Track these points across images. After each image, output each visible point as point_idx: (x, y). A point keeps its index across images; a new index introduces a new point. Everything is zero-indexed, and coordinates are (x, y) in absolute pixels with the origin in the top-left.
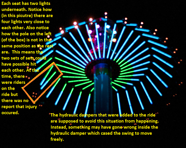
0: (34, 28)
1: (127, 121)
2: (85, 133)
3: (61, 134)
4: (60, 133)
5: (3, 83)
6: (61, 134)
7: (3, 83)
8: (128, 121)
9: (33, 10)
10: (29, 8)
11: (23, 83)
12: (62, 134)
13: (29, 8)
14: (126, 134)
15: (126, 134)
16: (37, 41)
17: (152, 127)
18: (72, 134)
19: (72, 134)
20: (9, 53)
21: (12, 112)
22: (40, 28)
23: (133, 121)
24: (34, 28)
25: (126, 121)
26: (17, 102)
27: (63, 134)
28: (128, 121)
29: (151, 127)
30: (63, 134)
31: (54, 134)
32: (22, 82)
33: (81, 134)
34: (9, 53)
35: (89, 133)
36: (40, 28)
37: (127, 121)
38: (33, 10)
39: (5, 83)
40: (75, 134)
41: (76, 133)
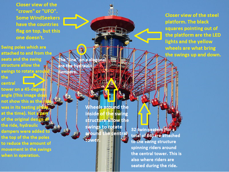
0: (138, 160)
1: (36, 53)
2: (178, 15)
3: (30, 126)
4: (28, 126)
5: (3, 108)
6: (30, 126)
7: (3, 108)
8: (37, 53)
9: (32, 114)
10: (29, 112)
11: (164, 160)
12: (30, 126)
13: (29, 112)
14: (178, 55)
15: (178, 55)
16: (7, 102)
17: (31, 137)
18: (2, 132)
19: (2, 132)
20: (177, 167)
21: (172, 141)
22: (5, 102)
23: (42, 53)
24: (138, 160)
25: (35, 53)
26: (4, 108)
27: (32, 126)
28: (37, 53)
29: (30, 138)
30: (32, 126)
31: (23, 126)
32: (163, 159)
33: (11, 132)
34: (177, 167)
35: (3, 155)
36: (5, 102)
37: (36, 53)
38: (32, 114)
39: (162, 154)
40: (5, 132)
41: (33, 143)
